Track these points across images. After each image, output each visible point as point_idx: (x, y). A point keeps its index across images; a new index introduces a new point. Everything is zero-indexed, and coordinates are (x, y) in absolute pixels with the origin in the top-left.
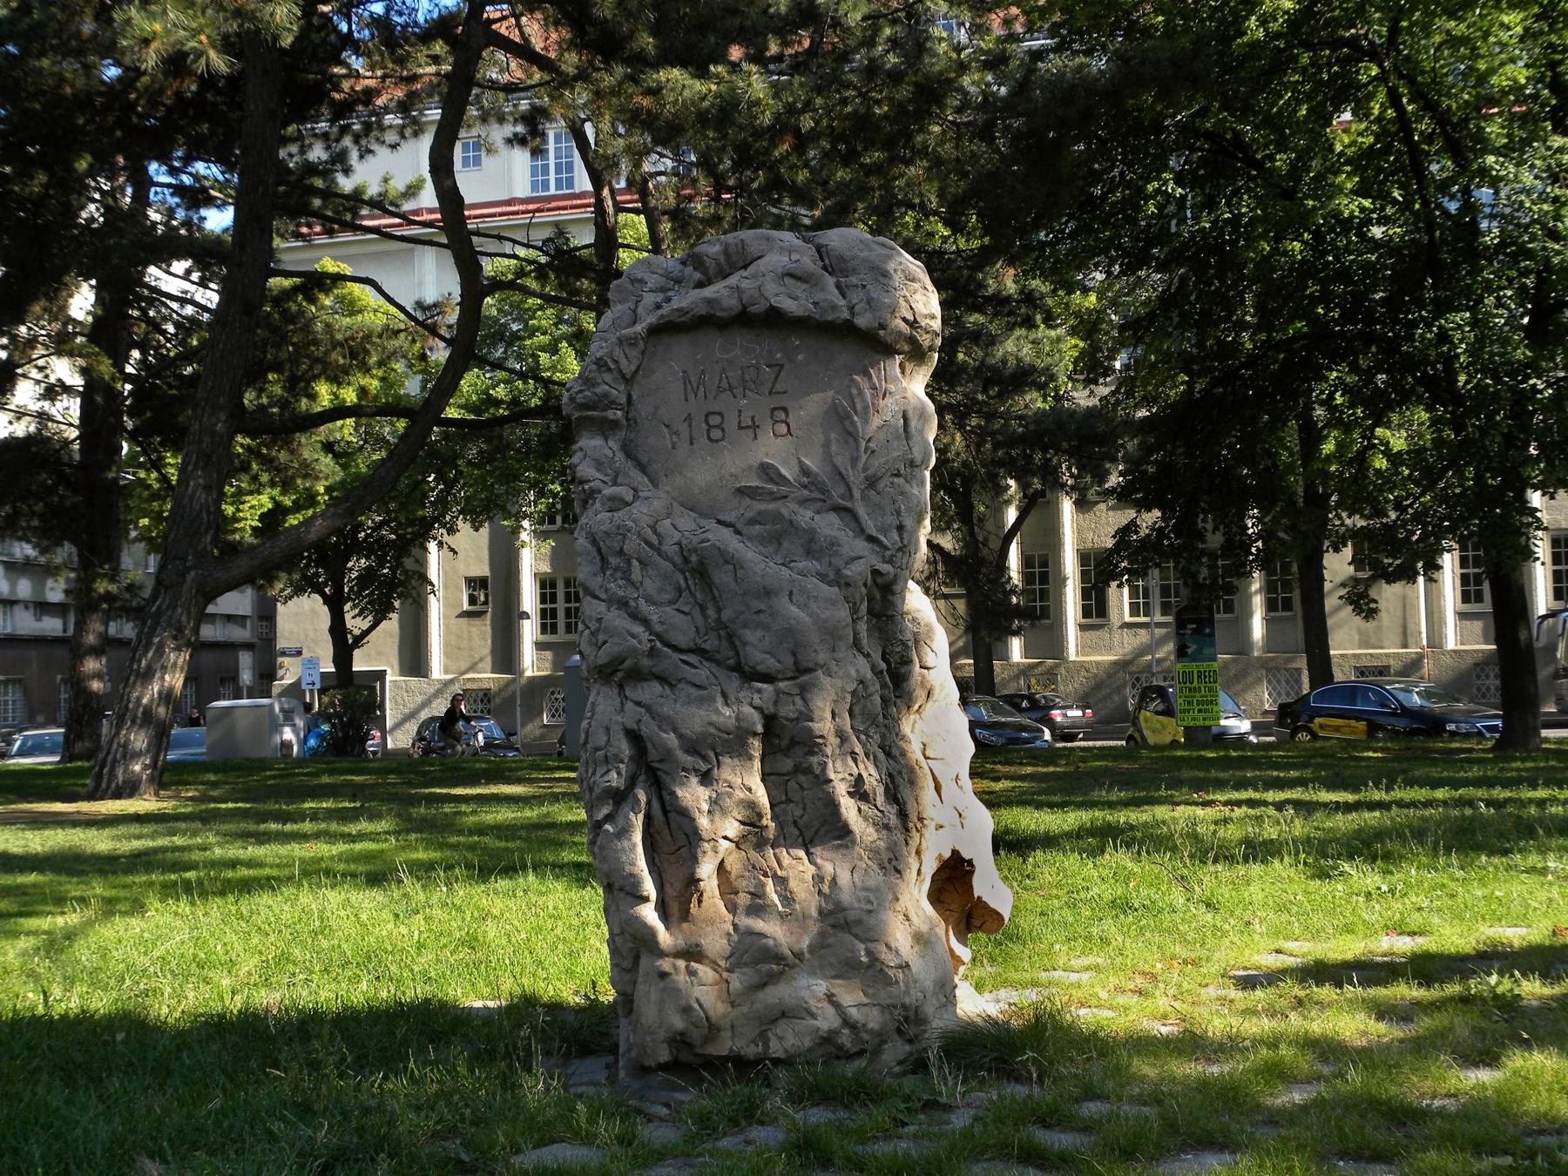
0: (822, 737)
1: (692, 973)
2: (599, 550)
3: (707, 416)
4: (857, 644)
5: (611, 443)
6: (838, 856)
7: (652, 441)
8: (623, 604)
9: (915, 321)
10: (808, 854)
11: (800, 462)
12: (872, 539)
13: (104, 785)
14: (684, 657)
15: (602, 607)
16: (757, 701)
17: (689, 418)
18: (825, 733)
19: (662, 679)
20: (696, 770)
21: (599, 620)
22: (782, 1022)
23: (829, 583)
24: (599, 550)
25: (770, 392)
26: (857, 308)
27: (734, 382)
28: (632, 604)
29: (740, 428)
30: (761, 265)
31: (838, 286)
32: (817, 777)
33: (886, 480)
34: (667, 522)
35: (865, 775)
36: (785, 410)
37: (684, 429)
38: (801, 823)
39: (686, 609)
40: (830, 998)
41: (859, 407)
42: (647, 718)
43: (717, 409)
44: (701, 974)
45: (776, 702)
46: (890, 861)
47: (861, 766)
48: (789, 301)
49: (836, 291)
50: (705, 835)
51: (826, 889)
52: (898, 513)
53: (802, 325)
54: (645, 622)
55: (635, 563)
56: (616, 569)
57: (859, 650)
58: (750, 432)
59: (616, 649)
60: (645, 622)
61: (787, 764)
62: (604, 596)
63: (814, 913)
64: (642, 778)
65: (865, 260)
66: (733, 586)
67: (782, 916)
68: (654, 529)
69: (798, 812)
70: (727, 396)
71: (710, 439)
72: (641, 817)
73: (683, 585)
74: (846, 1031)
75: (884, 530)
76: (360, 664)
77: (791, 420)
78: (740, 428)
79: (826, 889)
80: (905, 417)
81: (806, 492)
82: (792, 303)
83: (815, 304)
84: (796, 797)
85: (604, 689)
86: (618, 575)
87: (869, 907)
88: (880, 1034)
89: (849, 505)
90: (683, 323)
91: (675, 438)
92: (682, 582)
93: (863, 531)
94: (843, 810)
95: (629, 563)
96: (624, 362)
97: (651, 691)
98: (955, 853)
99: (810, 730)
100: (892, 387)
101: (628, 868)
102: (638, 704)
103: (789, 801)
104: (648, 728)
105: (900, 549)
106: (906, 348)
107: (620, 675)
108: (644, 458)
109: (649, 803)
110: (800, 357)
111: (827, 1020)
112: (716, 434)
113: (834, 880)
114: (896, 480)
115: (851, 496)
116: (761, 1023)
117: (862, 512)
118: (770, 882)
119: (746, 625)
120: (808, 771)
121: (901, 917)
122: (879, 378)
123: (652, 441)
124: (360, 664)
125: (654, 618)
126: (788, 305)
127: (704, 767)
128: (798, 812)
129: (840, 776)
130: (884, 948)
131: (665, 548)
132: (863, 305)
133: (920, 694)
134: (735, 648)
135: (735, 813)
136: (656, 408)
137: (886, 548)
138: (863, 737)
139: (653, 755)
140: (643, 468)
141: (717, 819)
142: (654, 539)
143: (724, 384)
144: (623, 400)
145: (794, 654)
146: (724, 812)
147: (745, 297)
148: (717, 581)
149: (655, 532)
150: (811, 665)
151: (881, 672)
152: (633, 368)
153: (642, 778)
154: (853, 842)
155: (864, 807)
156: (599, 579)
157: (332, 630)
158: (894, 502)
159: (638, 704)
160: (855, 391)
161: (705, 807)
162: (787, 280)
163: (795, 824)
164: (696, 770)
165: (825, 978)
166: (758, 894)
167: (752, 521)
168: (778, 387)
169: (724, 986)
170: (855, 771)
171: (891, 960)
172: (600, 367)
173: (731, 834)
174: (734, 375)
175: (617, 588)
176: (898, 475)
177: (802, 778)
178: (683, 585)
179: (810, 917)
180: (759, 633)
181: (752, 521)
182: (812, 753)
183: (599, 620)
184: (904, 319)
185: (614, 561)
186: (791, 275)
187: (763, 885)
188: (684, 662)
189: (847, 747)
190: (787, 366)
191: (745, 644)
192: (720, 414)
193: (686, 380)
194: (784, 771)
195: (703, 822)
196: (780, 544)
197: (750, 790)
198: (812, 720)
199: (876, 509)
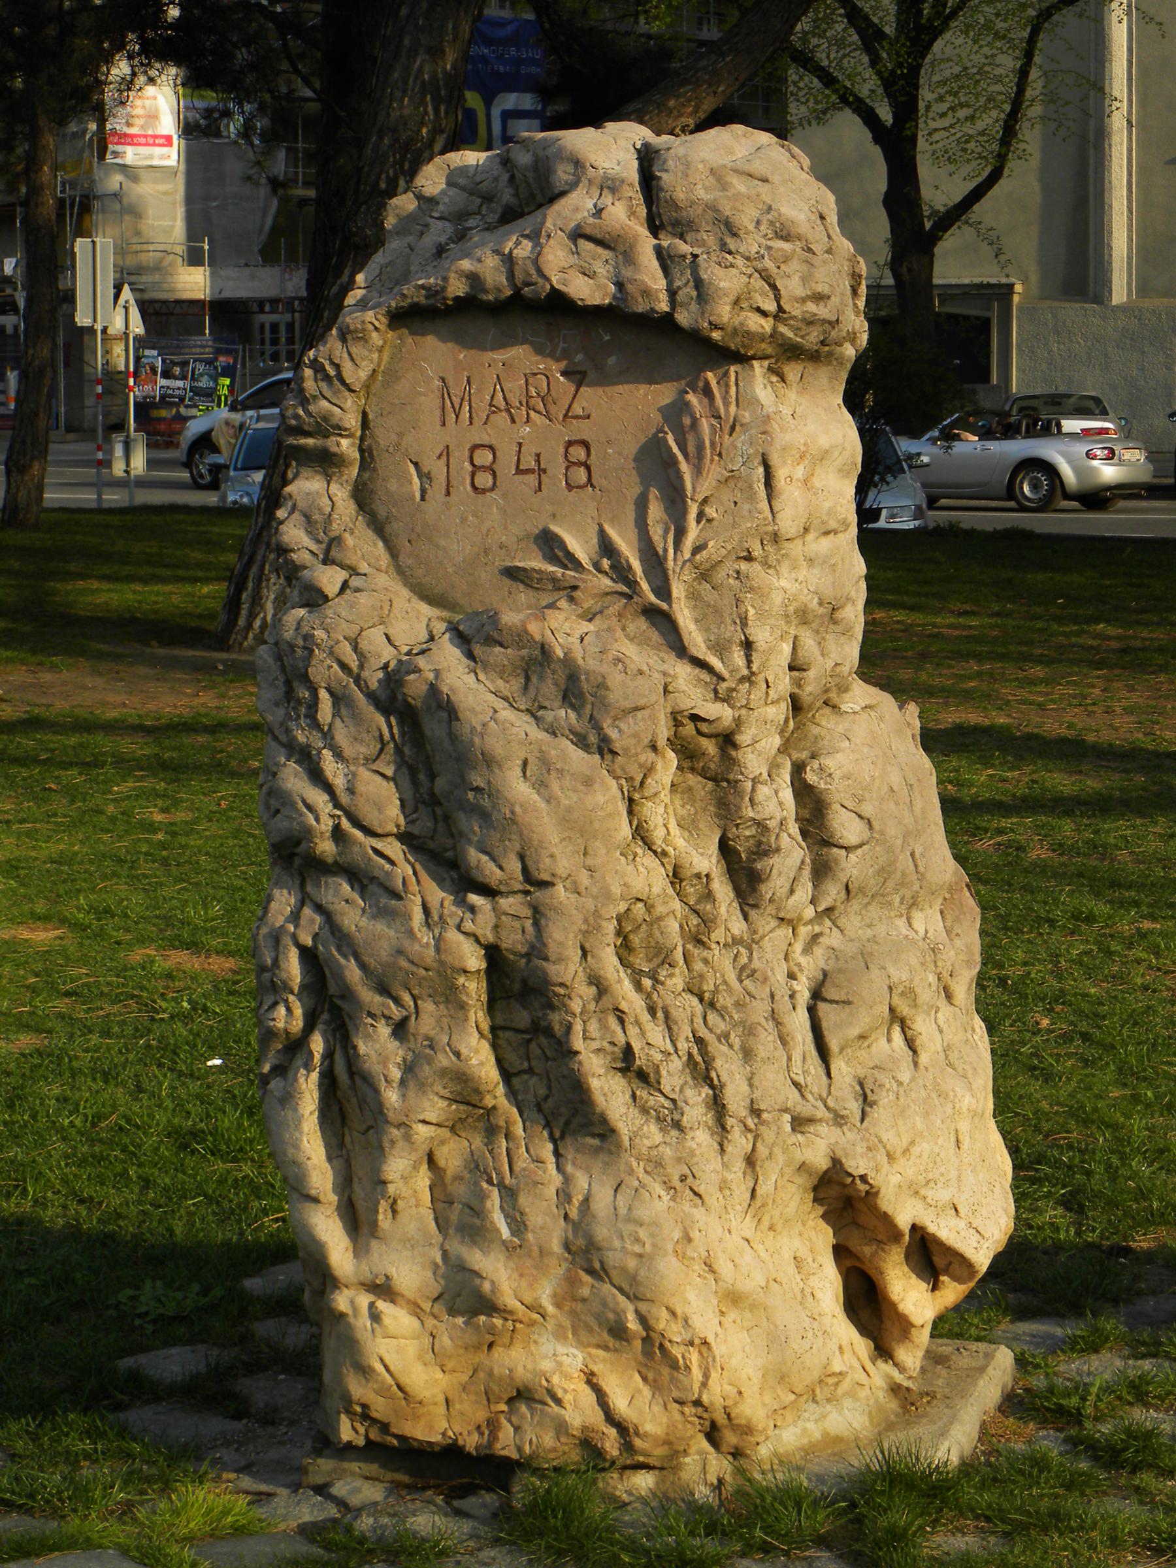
0: (562, 985)
1: (375, 1317)
2: (1032, 41)
5: (334, 487)
6: (597, 1166)
10: (557, 1154)
11: (602, 533)
13: (242, 622)
18: (567, 979)
20: (388, 1018)
24: (1032, 41)
26: (681, 296)
29: (519, 471)
32: (559, 1043)
33: (729, 567)
35: (637, 1046)
36: (585, 444)
40: (591, 1380)
41: (691, 449)
43: (486, 440)
44: (386, 1320)
45: (496, 927)
46: (683, 1178)
47: (632, 1030)
49: (655, 263)
50: (391, 1115)
51: (574, 1213)
52: (744, 623)
55: (323, 694)
57: (649, 845)
58: (532, 479)
61: (522, 1018)
62: (283, 738)
63: (556, 1247)
64: (325, 1016)
67: (508, 1247)
72: (315, 1076)
76: (955, 265)
77: (593, 461)
78: (519, 471)
79: (574, 1213)
88: (667, 1442)
94: (598, 1098)
98: (836, 1162)
99: (545, 973)
100: (746, 417)
101: (290, 1151)
103: (530, 1071)
105: (743, 679)
106: (770, 350)
108: (382, 513)
109: (329, 1055)
110: (611, 360)
111: (579, 1410)
113: (586, 1200)
114: (744, 566)
117: (685, 617)
118: (495, 1193)
120: (548, 1031)
121: (698, 1267)
122: (727, 404)
124: (955, 265)
127: (396, 1013)
128: (542, 1091)
129: (595, 1045)
130: (664, 1314)
131: (365, 674)
135: (438, 1088)
136: (401, 435)
137: (721, 678)
138: (647, 983)
139: (333, 989)
140: (379, 526)
141: (411, 1094)
146: (422, 1086)
147: (519, 276)
148: (428, 733)
149: (356, 648)
150: (545, 877)
153: (325, 1016)
154: (619, 1145)
155: (642, 1093)
156: (281, 712)
157: (890, 201)
158: (738, 601)
160: (687, 421)
161: (396, 1074)
164: (388, 1018)
166: (476, 1210)
169: (427, 1341)
170: (621, 1039)
171: (675, 1332)
173: (431, 1116)
174: (515, 387)
176: (749, 558)
179: (550, 1253)
182: (551, 1007)
187: (483, 1197)
189: (606, 1002)
195: (392, 1097)
197: (458, 1054)
198: (546, 959)
199: (707, 615)
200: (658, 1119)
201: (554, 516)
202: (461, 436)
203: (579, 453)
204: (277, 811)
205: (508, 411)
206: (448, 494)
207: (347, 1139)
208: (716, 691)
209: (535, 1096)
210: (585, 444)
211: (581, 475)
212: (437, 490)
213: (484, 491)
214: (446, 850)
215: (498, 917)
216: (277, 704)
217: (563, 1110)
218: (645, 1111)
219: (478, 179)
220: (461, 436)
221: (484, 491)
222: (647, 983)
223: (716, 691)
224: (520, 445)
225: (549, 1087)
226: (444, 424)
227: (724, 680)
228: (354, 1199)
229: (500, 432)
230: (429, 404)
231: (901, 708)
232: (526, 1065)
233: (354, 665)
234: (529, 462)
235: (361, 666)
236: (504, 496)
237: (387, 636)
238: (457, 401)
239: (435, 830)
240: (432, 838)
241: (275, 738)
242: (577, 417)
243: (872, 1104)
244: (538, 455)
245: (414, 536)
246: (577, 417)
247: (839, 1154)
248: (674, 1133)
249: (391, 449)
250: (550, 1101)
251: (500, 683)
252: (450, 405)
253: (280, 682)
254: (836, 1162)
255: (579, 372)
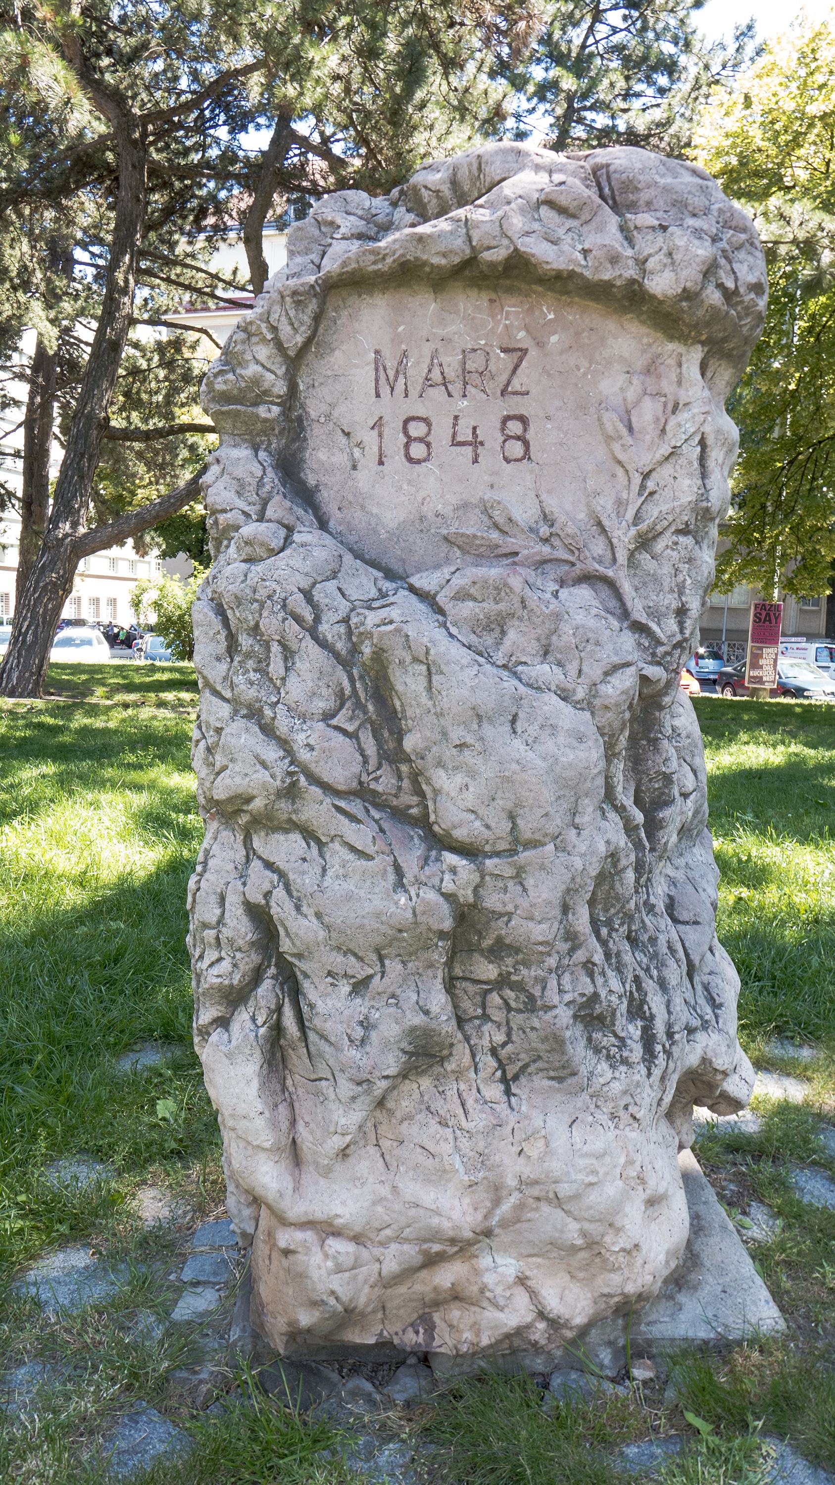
2: (226, 622)
3: (406, 422)
4: (609, 795)
7: (322, 455)
8: (254, 713)
9: (736, 292)
12: (639, 628)
14: (342, 804)
15: (225, 710)
16: (448, 886)
17: (378, 425)
19: (309, 834)
21: (219, 731)
22: (454, 1305)
23: (577, 705)
24: (226, 622)
25: (503, 393)
26: (650, 265)
27: (450, 374)
28: (268, 712)
30: (508, 188)
31: (623, 229)
34: (331, 585)
36: (426, 421)
37: (370, 438)
38: (503, 1053)
39: (350, 728)
42: (279, 893)
43: (422, 413)
47: (600, 981)
48: (546, 245)
49: (619, 236)
53: (564, 284)
54: (285, 744)
55: (275, 648)
56: (248, 655)
59: (238, 780)
60: (285, 744)
62: (228, 694)
64: (272, 971)
65: (666, 190)
66: (424, 699)
68: (308, 595)
69: (500, 1038)
70: (438, 393)
71: (410, 460)
73: (348, 691)
74: (541, 1325)
75: (655, 613)
78: (455, 443)
80: (702, 443)
81: (546, 550)
82: (551, 254)
83: (585, 252)
84: (498, 1015)
85: (226, 834)
86: (251, 664)
87: (592, 1179)
89: (610, 573)
90: (377, 273)
91: (357, 452)
92: (346, 683)
93: (625, 614)
95: (268, 649)
96: (285, 330)
97: (285, 848)
102: (269, 865)
104: (281, 908)
105: (678, 645)
107: (244, 819)
111: (516, 1314)
112: (417, 451)
115: (614, 560)
116: (425, 1305)
117: (626, 587)
119: (440, 764)
123: (322, 455)
125: (300, 738)
126: (539, 250)
128: (500, 1038)
129: (568, 997)
132: (661, 256)
133: (773, 1049)
134: (422, 794)
137: (659, 643)
139: (285, 945)
142: (307, 614)
143: (436, 375)
144: (281, 388)
145: (512, 817)
147: (476, 235)
148: (399, 687)
151: (637, 827)
152: (300, 339)
153: (272, 971)
156: (223, 667)
159: (269, 865)
162: (544, 211)
163: (494, 1052)
165: (520, 1256)
167: (462, 596)
168: (516, 385)
170: (589, 990)
172: (250, 335)
174: (451, 362)
175: (247, 687)
177: (509, 994)
178: (348, 691)
180: (459, 779)
181: (462, 596)
183: (219, 731)
184: (720, 286)
185: (245, 642)
186: (550, 203)
188: (339, 809)
189: (580, 956)
190: (533, 352)
191: (436, 792)
192: (426, 421)
193: (378, 365)
194: (483, 977)
196: (503, 633)
197: (427, 1013)
200: (608, 1057)
201: (492, 486)
202: (394, 409)
203: (515, 427)
204: (224, 768)
205: (444, 384)
206: (381, 463)
207: (289, 1082)
208: (654, 655)
209: (491, 1041)
210: (523, 420)
211: (516, 449)
212: (368, 461)
213: (419, 462)
214: (411, 807)
215: (482, 877)
216: (218, 659)
217: (523, 1056)
218: (597, 1051)
219: (374, 211)
220: (394, 409)
221: (419, 462)
222: (604, 931)
223: (654, 655)
224: (456, 418)
225: (509, 1035)
226: (378, 395)
227: (663, 644)
228: (299, 1141)
229: (435, 406)
230: (364, 376)
231: (410, 731)
232: (480, 1011)
233: (309, 617)
234: (465, 434)
235: (317, 619)
236: (441, 466)
237: (339, 589)
238: (391, 374)
239: (399, 788)
240: (396, 796)
241: (216, 693)
242: (515, 393)
243: (721, 1005)
244: (475, 428)
245: (345, 503)
246: (515, 393)
247: (710, 1054)
248: (623, 1068)
249: (322, 420)
250: (509, 1047)
251: (473, 637)
252: (387, 376)
253: (222, 637)
254: (705, 1060)
255: (521, 350)
